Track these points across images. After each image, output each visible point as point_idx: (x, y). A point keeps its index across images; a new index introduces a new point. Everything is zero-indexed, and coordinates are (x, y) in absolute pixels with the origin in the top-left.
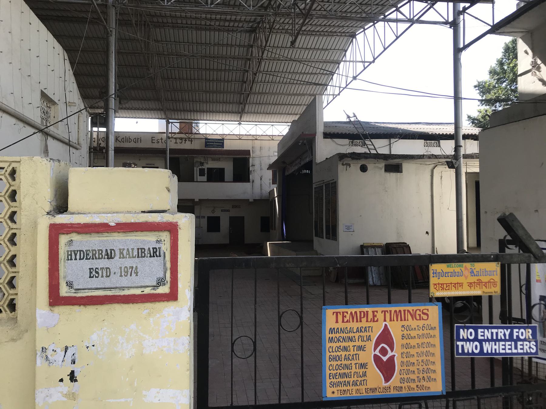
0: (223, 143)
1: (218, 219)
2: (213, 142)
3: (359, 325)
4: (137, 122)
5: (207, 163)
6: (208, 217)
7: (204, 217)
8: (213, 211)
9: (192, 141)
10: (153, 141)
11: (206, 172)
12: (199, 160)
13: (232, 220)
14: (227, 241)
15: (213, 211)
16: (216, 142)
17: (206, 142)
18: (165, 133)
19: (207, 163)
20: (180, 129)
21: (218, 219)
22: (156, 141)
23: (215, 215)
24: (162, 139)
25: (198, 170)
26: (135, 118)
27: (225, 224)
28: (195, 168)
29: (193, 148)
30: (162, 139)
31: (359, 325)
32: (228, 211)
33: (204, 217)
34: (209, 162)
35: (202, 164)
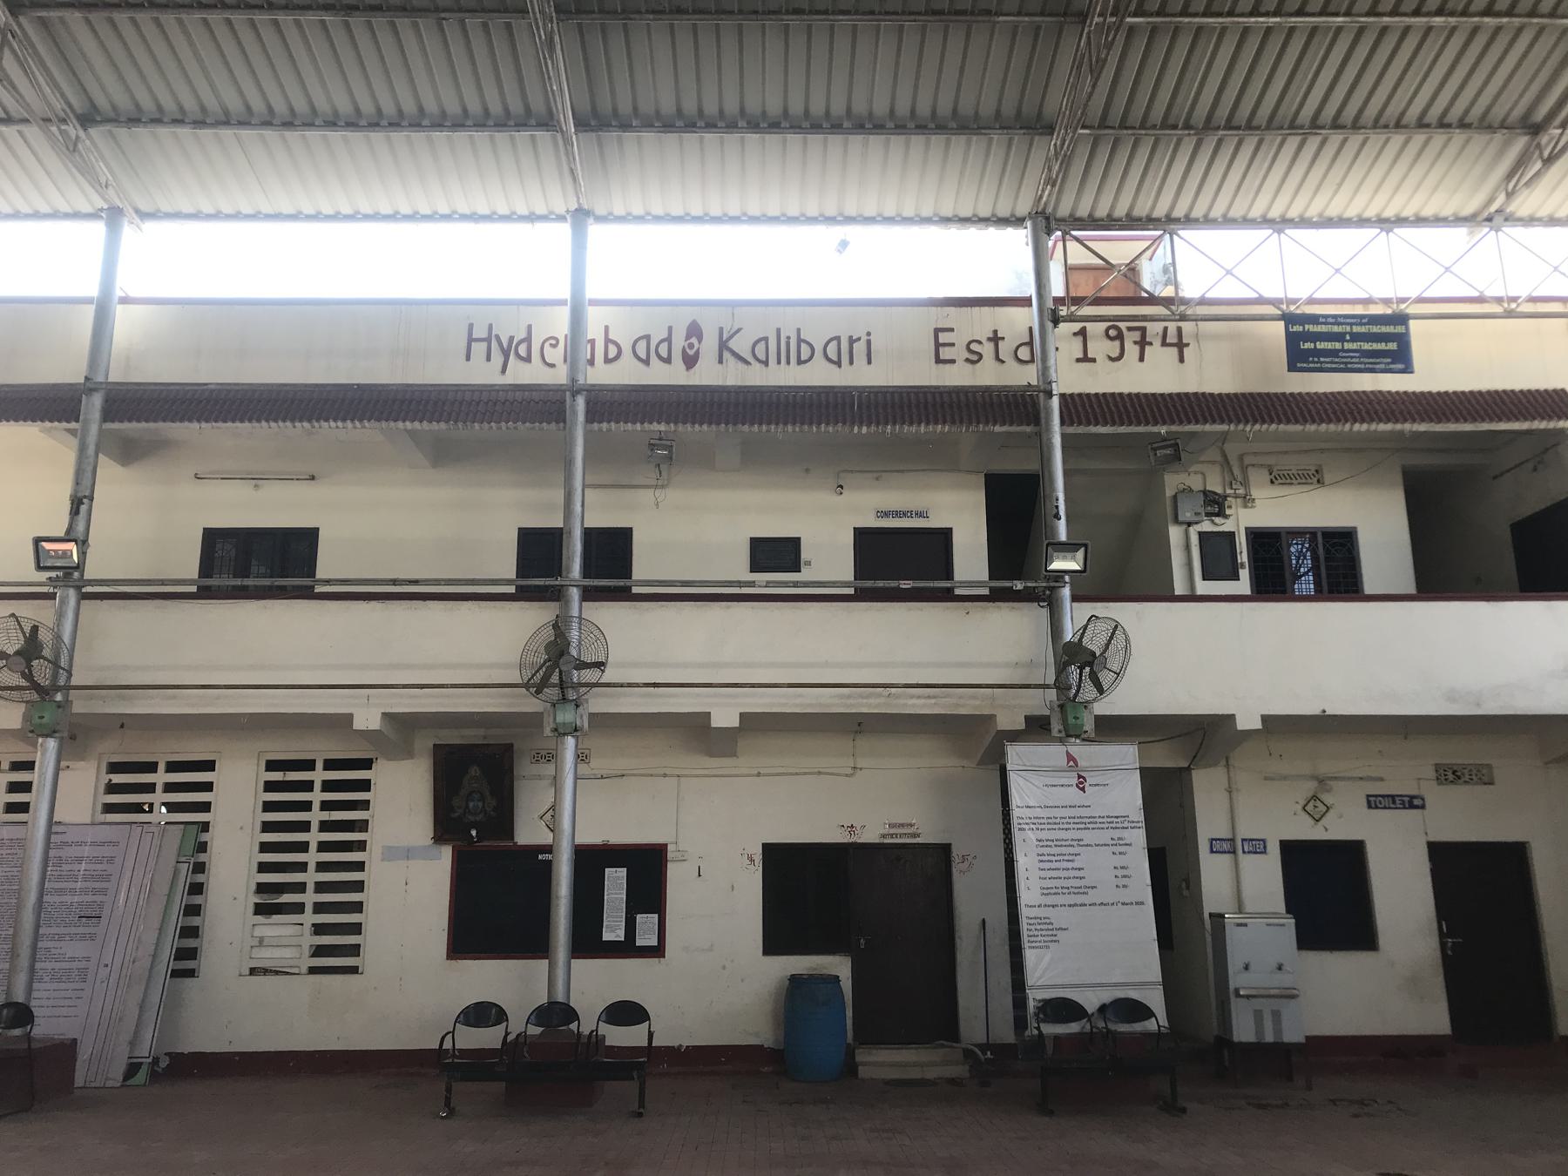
0: (1403, 341)
1: (1351, 856)
2: (1339, 337)
3: (64, 898)
4: (844, 244)
5: (1247, 501)
6: (1287, 848)
7: (1258, 847)
8: (1315, 807)
9: (1181, 346)
10: (945, 353)
11: (1243, 557)
12: (1195, 483)
13: (1453, 866)
14: (1434, 1018)
15: (1315, 807)
16: (1356, 337)
17: (1292, 340)
18: (1025, 302)
19: (1247, 501)
20: (27, 718)
21: (1351, 856)
22: (959, 353)
23: (1335, 829)
24: (995, 339)
25: (1194, 540)
26: (830, 220)
27: (1402, 894)
28: (1175, 533)
29: (1191, 387)
30: (995, 339)
31: (64, 898)
32: (1412, 803)
33: (1258, 847)
34: (1255, 493)
35: (1215, 505)
